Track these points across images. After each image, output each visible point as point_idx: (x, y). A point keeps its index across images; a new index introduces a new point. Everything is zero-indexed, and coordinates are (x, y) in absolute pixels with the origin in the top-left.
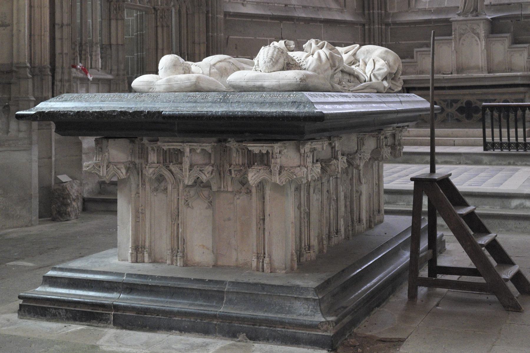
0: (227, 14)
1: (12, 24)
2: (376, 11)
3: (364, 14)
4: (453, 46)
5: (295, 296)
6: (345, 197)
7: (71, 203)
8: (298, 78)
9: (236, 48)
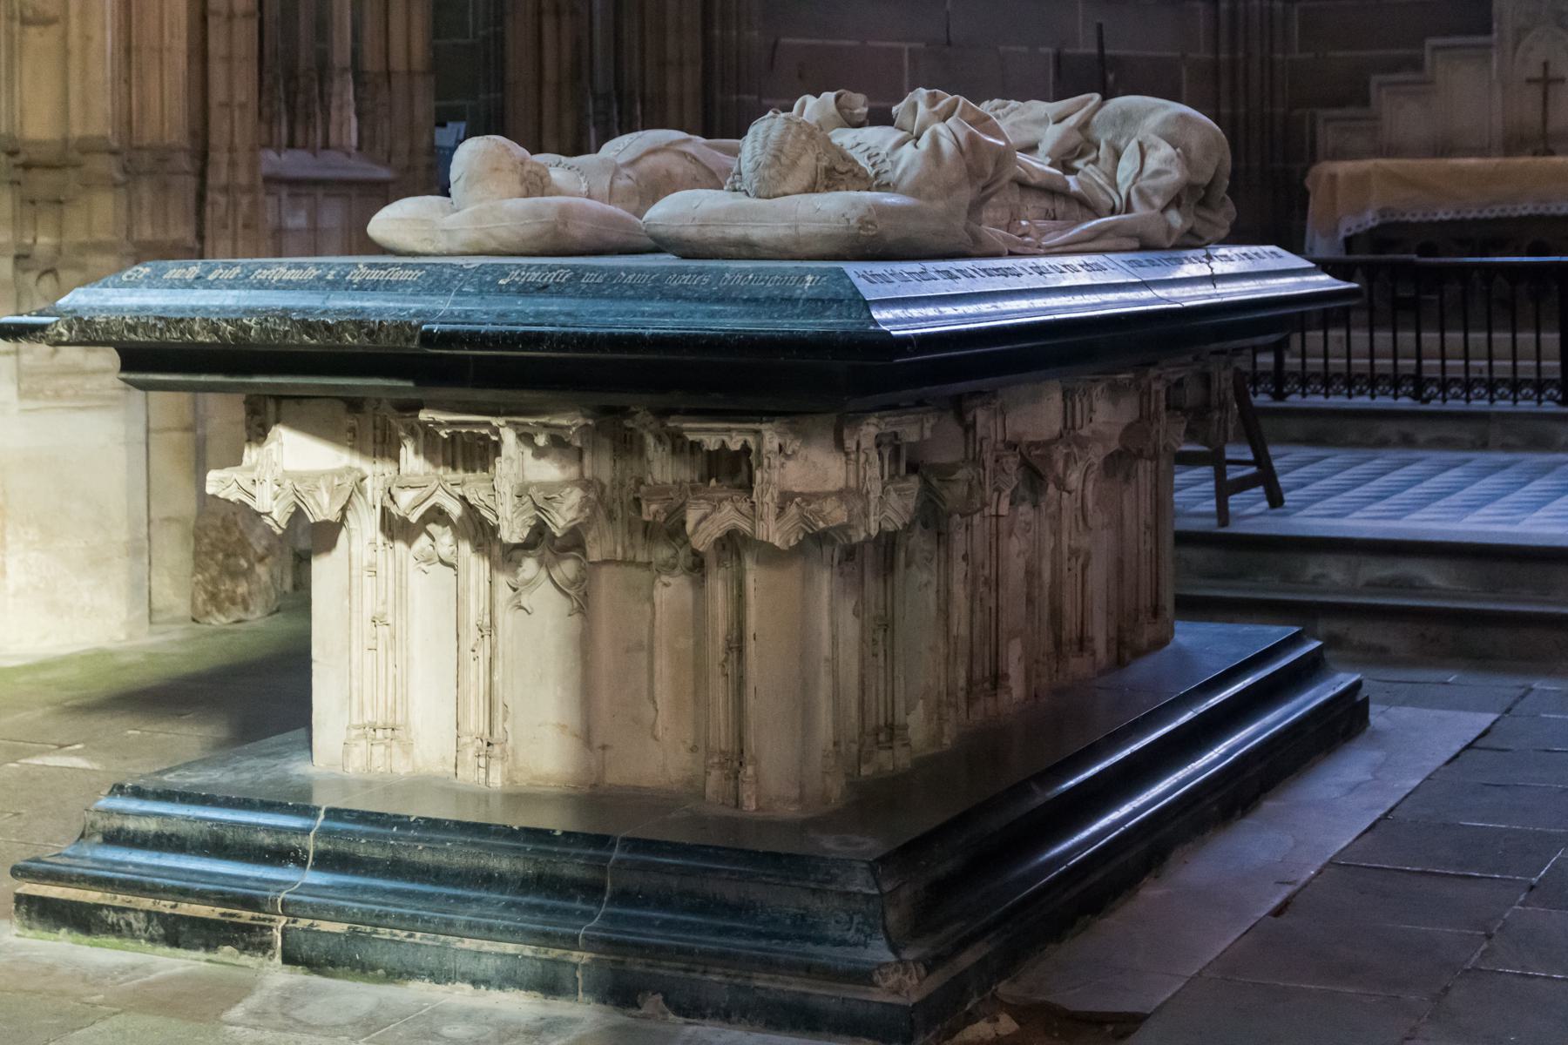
1: (67, 19)
4: (1495, 65)
5: (813, 885)
6: (1027, 572)
7: (251, 567)
8: (853, 215)
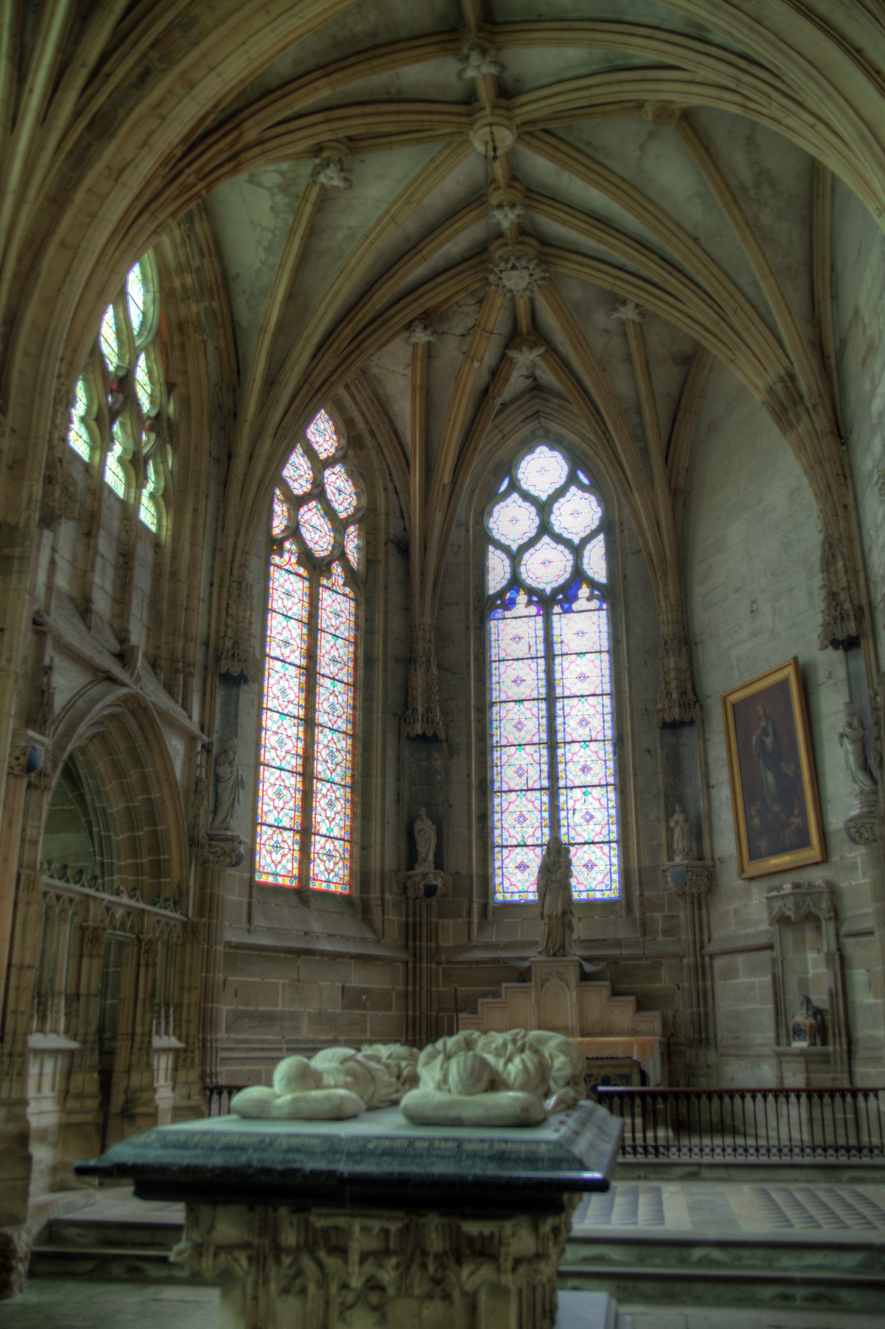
0: (229, 945)
2: (424, 944)
3: (407, 946)
9: (236, 995)
